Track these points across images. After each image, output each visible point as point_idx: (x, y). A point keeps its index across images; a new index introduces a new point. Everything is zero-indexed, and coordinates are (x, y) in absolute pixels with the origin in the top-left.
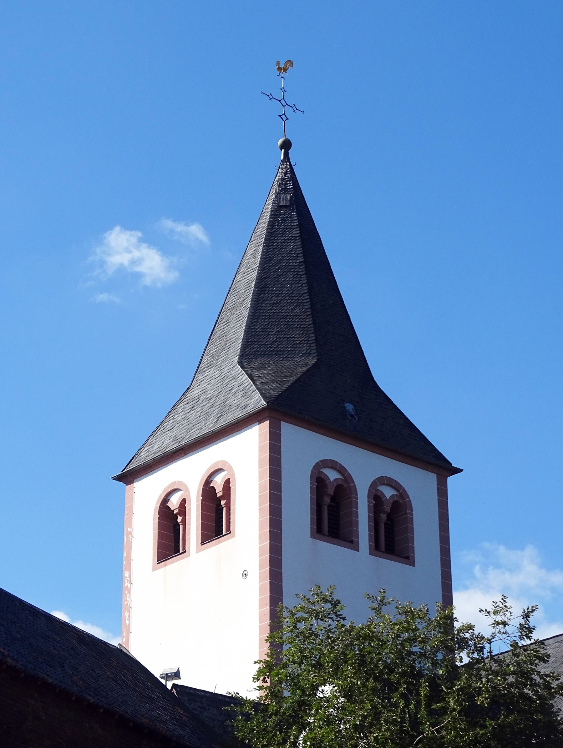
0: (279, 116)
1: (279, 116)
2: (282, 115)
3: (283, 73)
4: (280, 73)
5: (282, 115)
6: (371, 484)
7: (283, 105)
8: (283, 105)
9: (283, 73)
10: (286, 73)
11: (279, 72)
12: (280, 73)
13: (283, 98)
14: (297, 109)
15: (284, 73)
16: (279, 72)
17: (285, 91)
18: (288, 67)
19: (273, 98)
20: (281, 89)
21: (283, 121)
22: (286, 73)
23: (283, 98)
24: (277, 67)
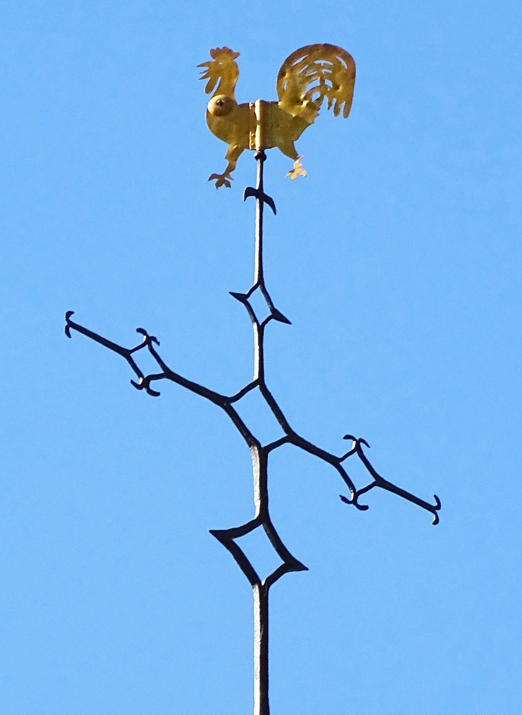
0: (298, 566)
1: (298, 566)
2: (264, 291)
3: (262, 157)
4: (234, 156)
5: (264, 291)
6: (199, 385)
7: (252, 441)
8: (252, 441)
9: (262, 157)
10: (294, 156)
11: (228, 147)
12: (234, 156)
13: (260, 382)
14: (380, 482)
15: (271, 153)
16: (228, 147)
17: (277, 315)
18: (313, 107)
19: (168, 374)
20: (242, 298)
21: (253, 578)
22: (294, 156)
23: (260, 382)
24: (211, 106)
